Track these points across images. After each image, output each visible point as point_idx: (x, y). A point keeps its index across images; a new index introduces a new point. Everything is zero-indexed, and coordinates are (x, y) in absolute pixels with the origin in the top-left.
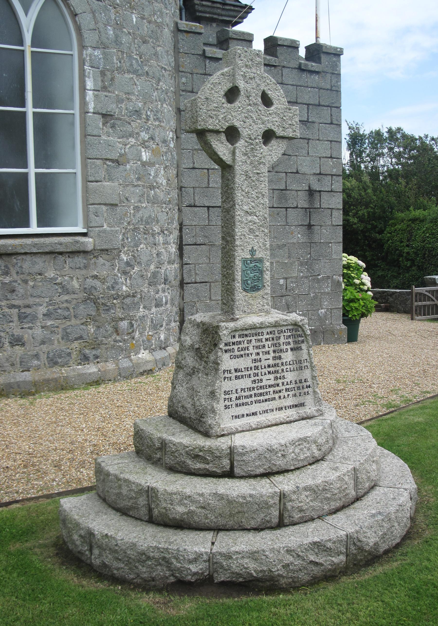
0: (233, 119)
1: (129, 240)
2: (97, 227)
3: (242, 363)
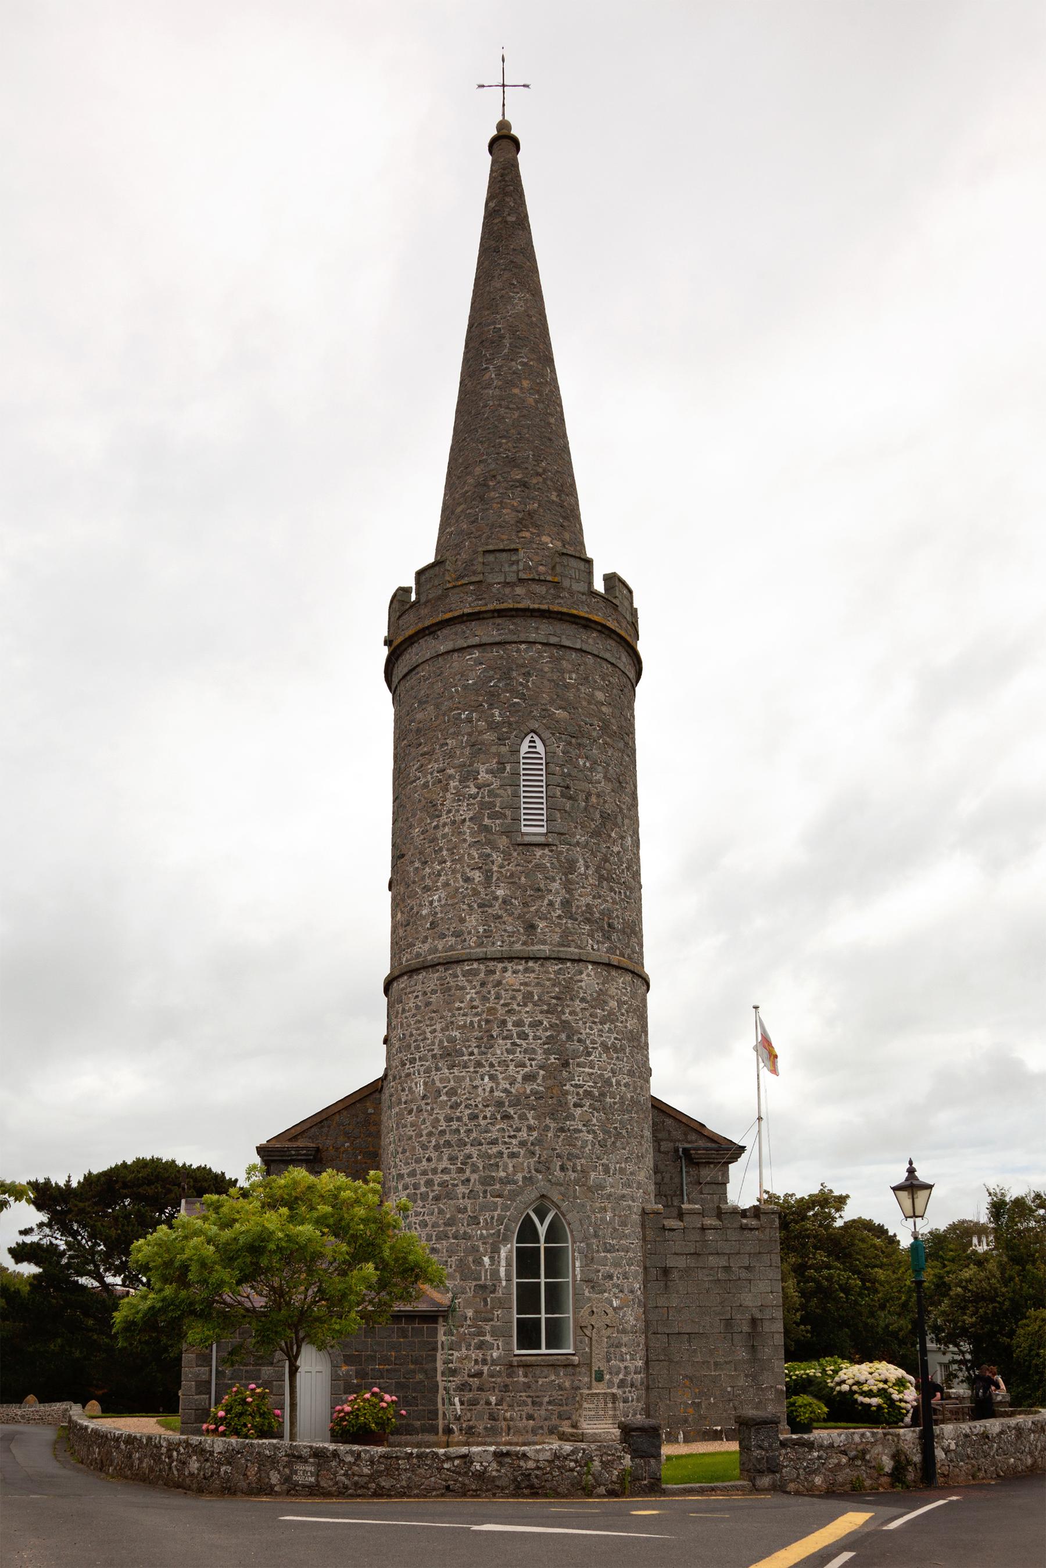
3: (591, 1406)
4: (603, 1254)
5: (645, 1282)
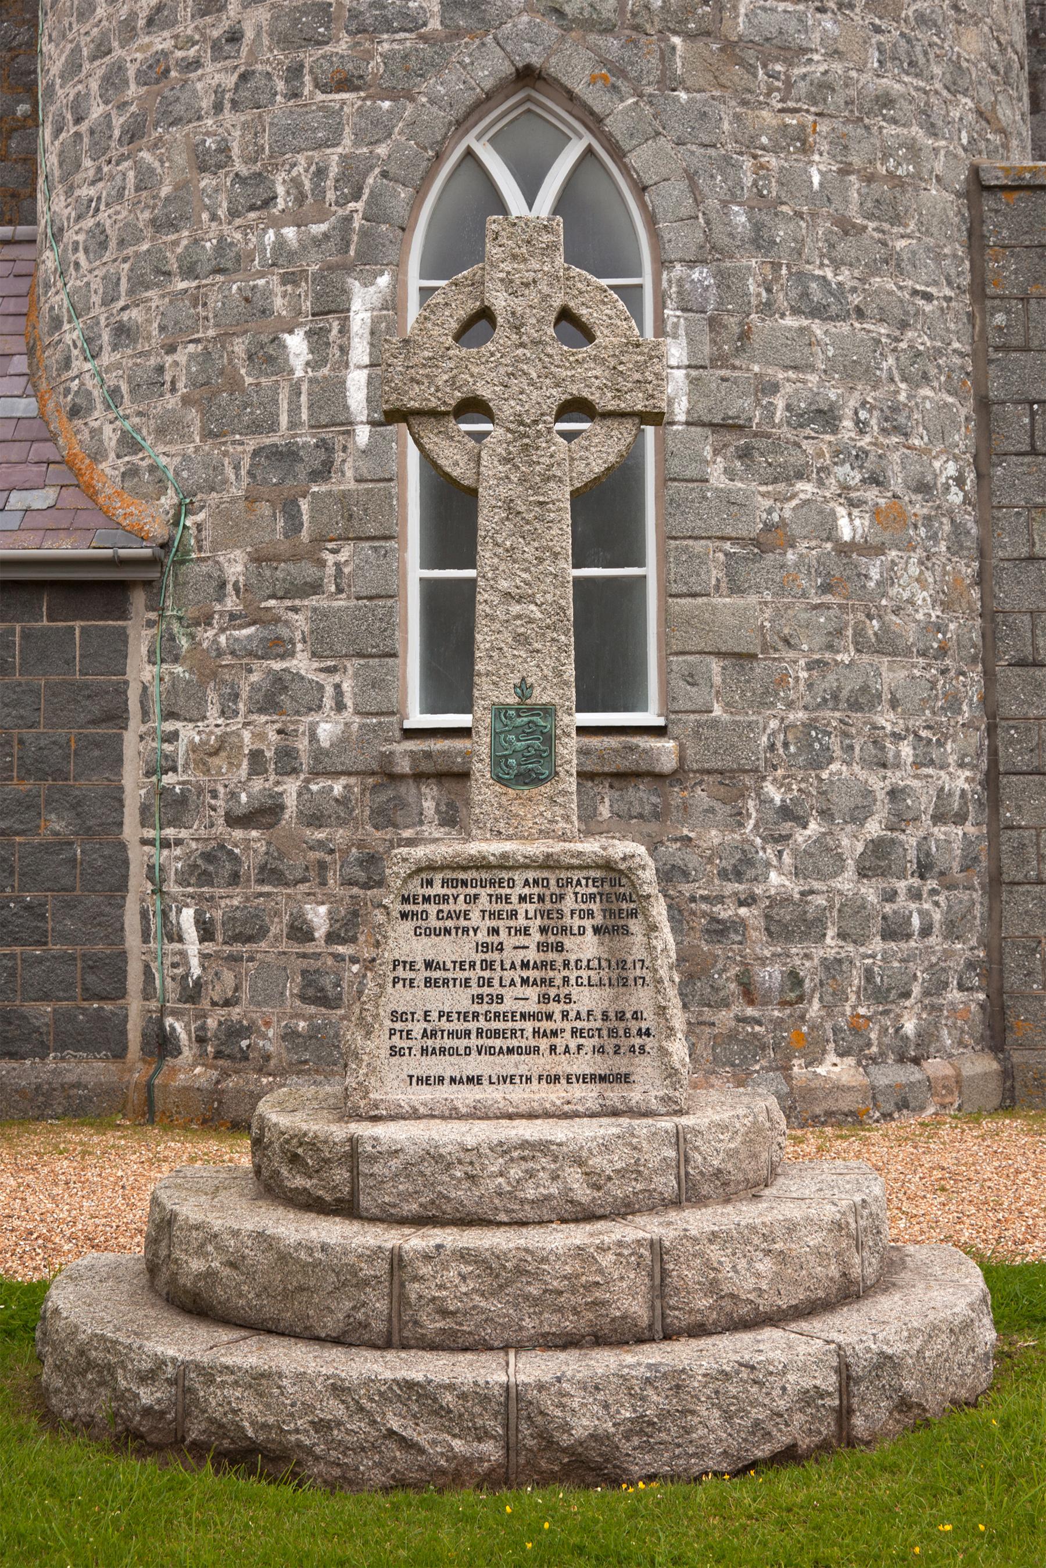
0: (475, 382)
1: (792, 749)
2: (693, 712)
3: (446, 949)
4: (790, 322)
5: (984, 459)
